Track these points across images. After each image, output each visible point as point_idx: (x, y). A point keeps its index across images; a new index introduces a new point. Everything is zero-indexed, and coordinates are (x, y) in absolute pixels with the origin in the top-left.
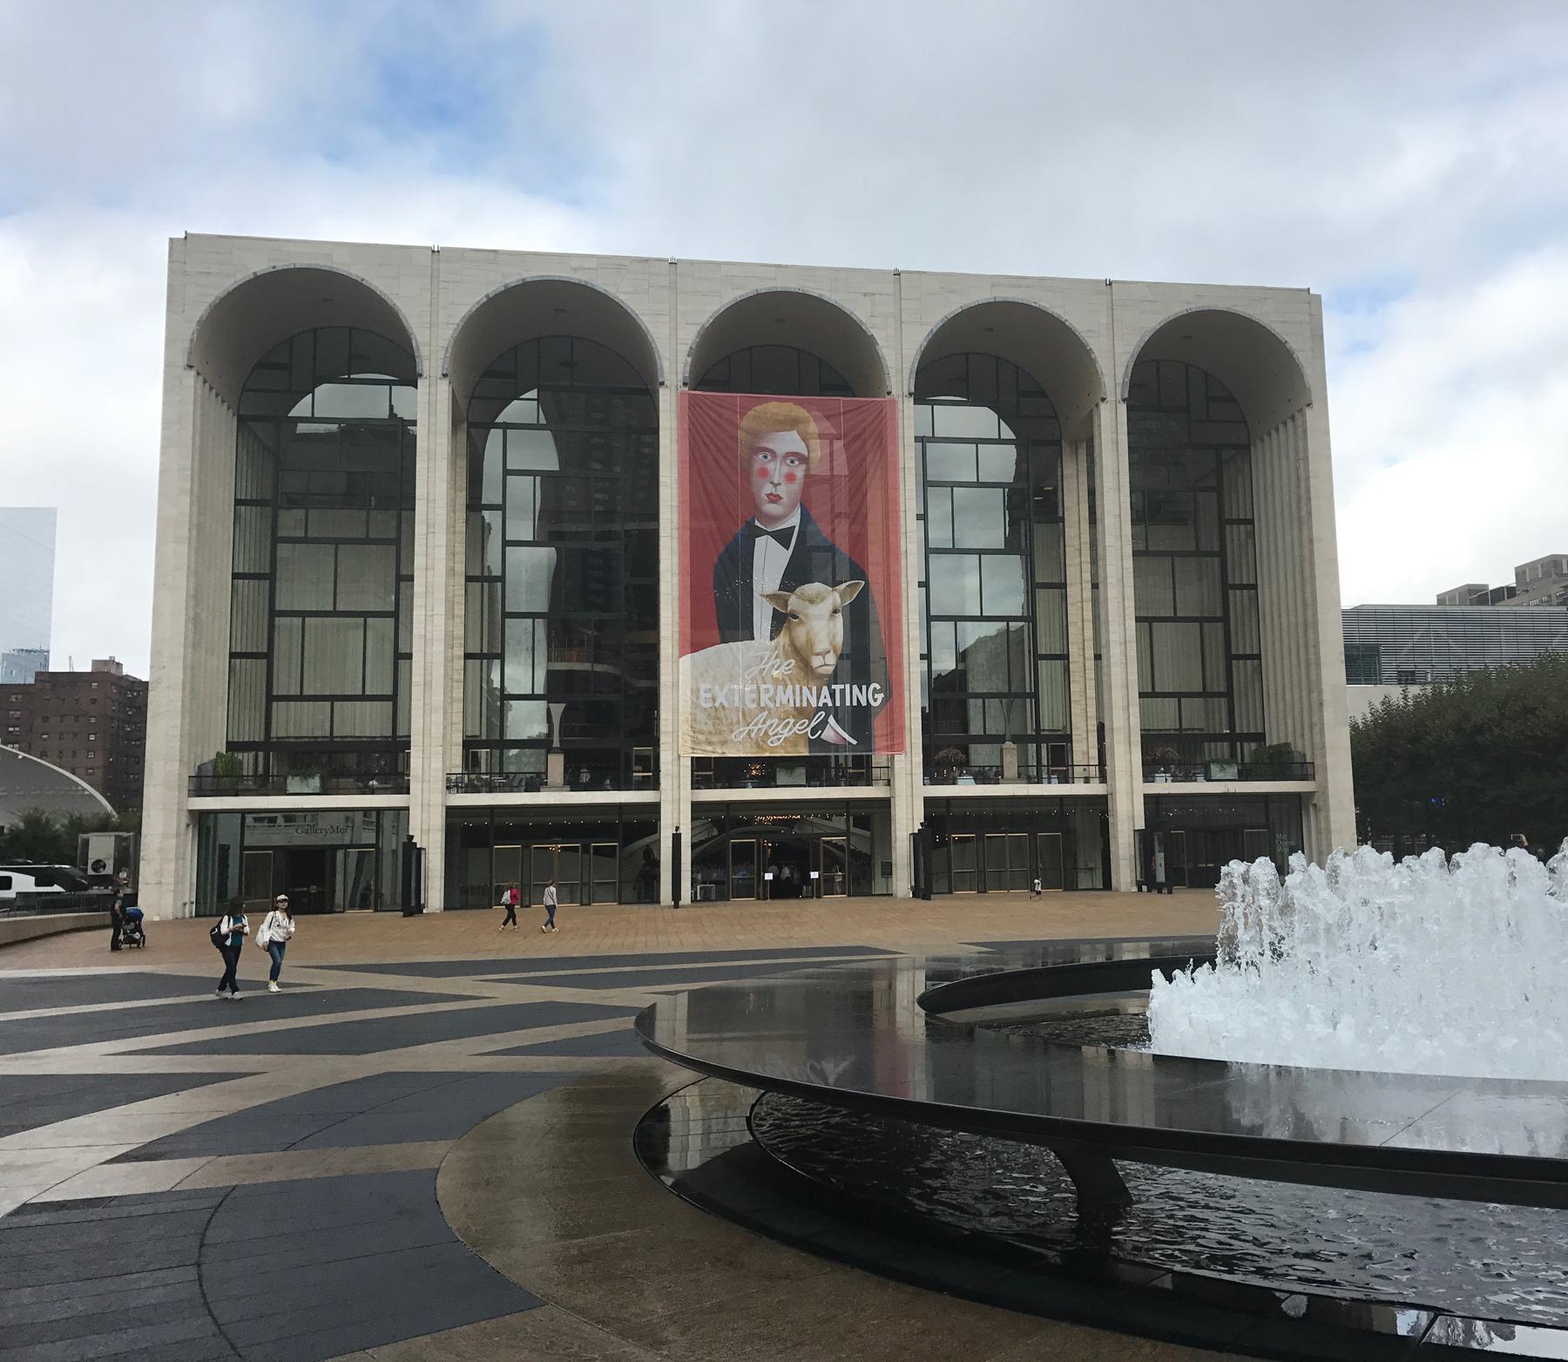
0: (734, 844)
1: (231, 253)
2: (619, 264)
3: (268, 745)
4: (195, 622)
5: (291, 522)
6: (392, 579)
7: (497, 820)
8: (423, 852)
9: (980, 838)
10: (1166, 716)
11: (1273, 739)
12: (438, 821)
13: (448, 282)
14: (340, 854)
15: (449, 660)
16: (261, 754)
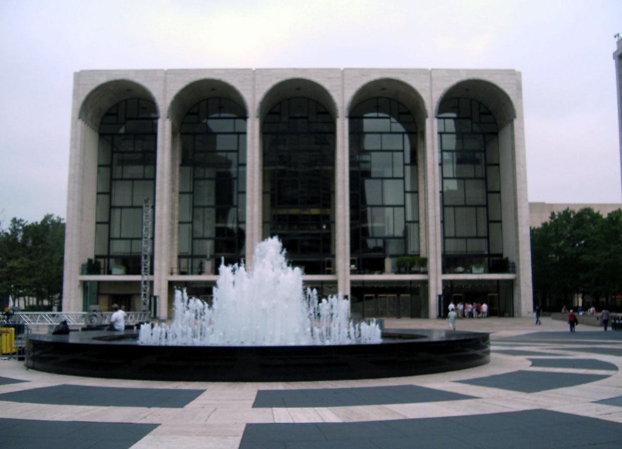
0: (490, 296)
3: (108, 257)
4: (81, 211)
5: (118, 171)
6: (402, 193)
7: (365, 285)
9: (376, 297)
10: (455, 247)
11: (505, 256)
12: (165, 286)
16: (106, 260)
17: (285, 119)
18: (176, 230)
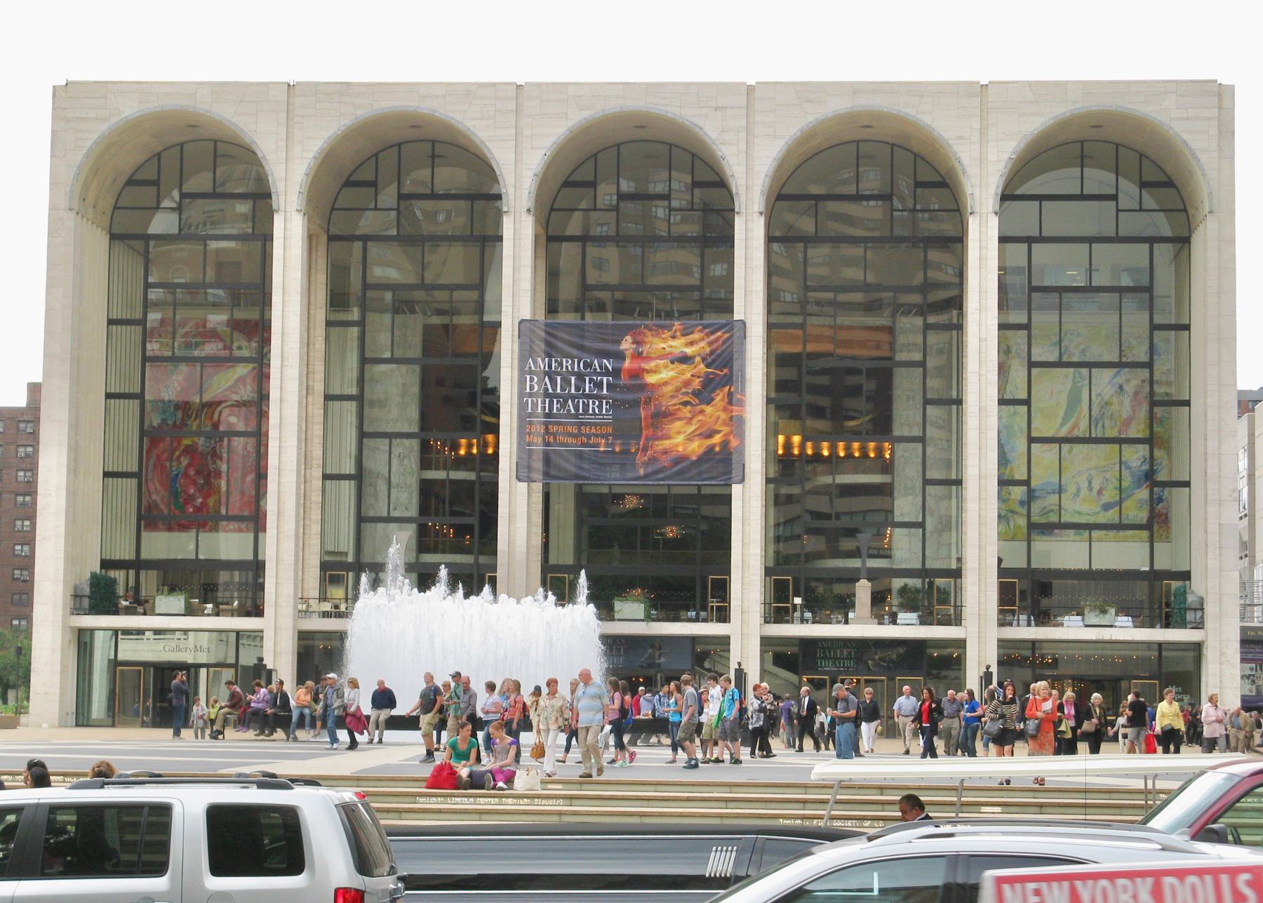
1: (106, 98)
2: (470, 92)
3: (137, 565)
8: (274, 673)
13: (303, 116)
14: (203, 671)
15: (304, 480)
16: (132, 573)
17: (388, 196)
18: (316, 497)
